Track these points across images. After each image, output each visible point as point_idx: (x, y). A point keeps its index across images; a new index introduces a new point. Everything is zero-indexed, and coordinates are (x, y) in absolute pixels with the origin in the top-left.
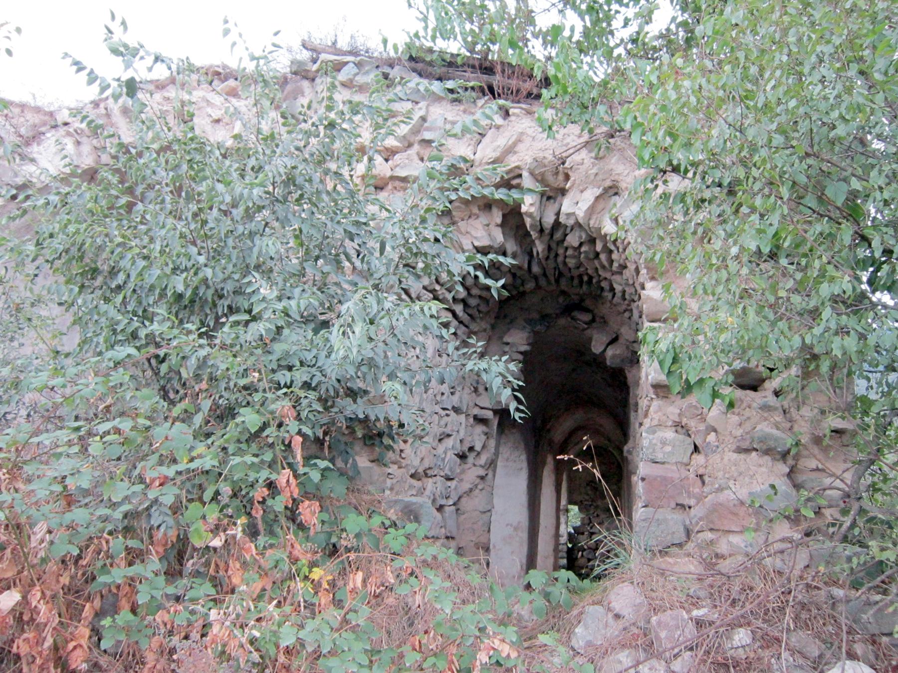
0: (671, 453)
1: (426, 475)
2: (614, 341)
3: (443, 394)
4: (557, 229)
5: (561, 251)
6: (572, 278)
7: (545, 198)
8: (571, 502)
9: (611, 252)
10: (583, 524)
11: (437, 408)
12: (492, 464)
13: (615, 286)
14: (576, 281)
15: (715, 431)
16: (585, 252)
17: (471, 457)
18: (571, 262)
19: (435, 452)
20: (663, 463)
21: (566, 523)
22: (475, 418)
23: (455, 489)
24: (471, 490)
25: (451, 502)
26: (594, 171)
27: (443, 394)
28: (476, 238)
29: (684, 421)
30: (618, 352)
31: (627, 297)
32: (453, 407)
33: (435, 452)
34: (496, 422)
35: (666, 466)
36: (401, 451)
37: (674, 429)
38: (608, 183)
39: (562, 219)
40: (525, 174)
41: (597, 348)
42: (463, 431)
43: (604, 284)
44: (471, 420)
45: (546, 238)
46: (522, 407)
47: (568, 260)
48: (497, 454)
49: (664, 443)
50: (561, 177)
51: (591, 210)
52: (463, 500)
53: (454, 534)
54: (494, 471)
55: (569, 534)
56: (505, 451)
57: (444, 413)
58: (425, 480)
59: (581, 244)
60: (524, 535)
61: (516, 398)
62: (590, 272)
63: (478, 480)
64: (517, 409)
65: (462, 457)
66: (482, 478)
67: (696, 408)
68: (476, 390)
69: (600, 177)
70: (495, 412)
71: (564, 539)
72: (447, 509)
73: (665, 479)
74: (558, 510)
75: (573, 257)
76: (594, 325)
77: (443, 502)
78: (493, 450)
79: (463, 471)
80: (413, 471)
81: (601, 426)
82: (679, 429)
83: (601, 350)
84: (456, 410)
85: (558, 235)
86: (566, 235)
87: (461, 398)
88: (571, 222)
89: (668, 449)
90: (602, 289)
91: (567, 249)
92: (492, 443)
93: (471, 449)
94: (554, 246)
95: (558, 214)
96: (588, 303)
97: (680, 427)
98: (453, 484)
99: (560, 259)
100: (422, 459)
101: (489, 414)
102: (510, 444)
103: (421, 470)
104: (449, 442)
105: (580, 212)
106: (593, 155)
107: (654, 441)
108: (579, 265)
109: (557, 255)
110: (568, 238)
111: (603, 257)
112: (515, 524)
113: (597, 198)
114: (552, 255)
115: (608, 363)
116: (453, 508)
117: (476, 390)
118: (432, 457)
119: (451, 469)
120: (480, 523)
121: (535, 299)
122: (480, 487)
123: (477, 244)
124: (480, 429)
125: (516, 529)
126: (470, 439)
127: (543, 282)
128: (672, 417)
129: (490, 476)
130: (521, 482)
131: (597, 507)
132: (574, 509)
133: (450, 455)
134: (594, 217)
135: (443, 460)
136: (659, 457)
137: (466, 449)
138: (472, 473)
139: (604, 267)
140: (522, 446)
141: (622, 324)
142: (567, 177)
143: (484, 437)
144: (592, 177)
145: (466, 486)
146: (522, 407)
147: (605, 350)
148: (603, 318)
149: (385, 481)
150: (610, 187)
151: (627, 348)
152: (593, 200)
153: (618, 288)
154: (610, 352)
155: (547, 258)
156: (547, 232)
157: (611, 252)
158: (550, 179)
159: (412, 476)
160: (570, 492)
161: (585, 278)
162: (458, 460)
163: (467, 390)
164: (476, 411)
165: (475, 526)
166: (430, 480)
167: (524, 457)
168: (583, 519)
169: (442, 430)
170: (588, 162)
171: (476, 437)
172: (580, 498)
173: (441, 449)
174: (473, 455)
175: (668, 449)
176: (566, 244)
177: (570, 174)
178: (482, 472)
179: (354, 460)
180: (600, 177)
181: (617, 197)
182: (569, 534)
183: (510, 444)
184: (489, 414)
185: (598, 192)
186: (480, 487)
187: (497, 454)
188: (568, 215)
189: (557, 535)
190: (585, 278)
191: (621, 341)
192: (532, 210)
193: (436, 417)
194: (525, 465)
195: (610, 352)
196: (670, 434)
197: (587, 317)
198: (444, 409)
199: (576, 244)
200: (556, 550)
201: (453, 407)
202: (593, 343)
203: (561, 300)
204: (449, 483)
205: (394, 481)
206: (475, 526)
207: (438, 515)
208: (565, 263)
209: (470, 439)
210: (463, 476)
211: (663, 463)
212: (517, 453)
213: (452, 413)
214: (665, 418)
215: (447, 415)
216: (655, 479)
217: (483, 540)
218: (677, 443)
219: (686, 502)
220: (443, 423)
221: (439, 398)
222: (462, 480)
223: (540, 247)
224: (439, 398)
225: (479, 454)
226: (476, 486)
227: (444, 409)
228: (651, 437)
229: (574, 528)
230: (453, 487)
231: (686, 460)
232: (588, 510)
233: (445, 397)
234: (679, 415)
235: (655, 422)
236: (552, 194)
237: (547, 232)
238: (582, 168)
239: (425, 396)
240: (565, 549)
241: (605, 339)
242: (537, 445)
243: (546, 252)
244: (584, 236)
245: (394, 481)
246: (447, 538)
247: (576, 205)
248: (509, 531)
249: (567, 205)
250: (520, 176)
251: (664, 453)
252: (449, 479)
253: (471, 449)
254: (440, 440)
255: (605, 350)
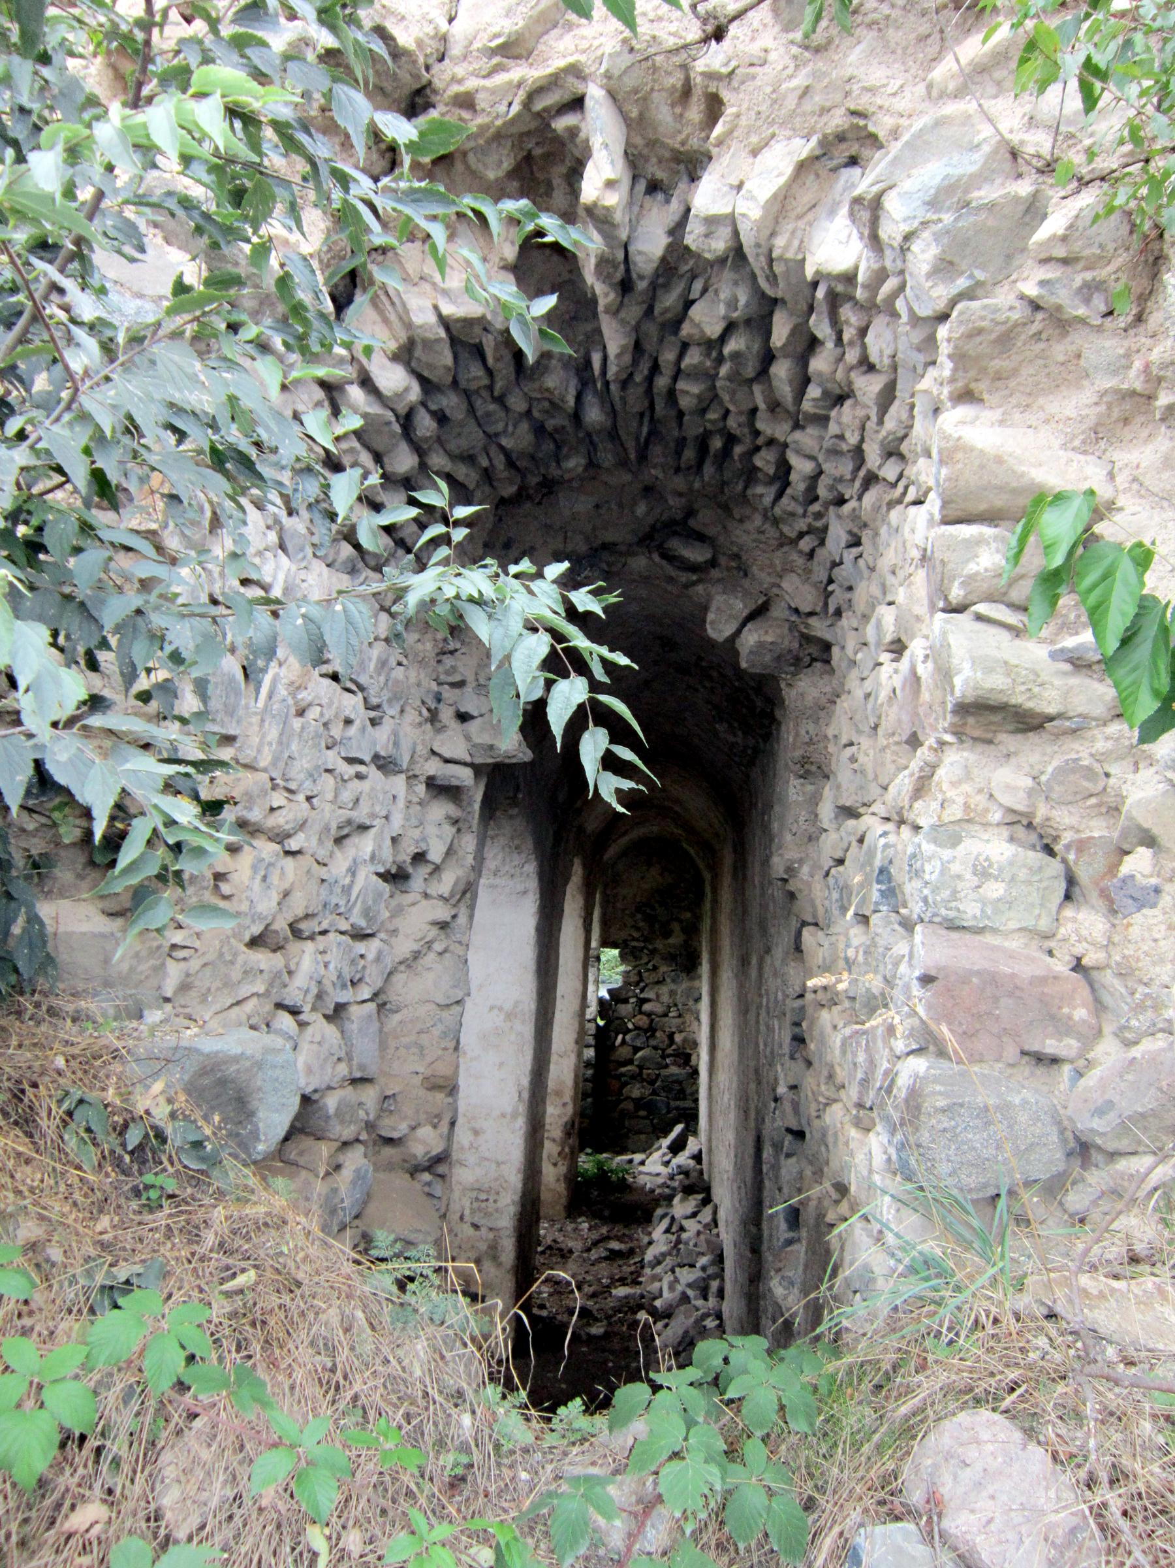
0: (1008, 903)
1: (296, 933)
2: (759, 612)
3: (348, 722)
4: (666, 286)
5: (668, 356)
6: (681, 443)
7: (642, 186)
8: (606, 943)
9: (813, 343)
10: (627, 983)
11: (332, 758)
12: (467, 892)
13: (793, 459)
14: (689, 454)
15: (1150, 841)
16: (736, 355)
17: (419, 876)
18: (690, 391)
19: (323, 872)
20: (980, 931)
21: (597, 982)
22: (431, 782)
23: (378, 959)
24: (417, 955)
25: (366, 993)
26: (800, 81)
27: (348, 722)
28: (445, 293)
29: (1042, 811)
30: (769, 639)
31: (822, 491)
32: (376, 757)
33: (323, 872)
34: (479, 796)
35: (989, 939)
36: (219, 877)
37: (1005, 832)
38: (837, 121)
39: (692, 237)
40: (595, 93)
41: (719, 627)
42: (400, 814)
43: (765, 461)
44: (421, 789)
45: (634, 312)
46: (625, 753)
47: (681, 385)
48: (478, 868)
49: (983, 873)
50: (695, 112)
51: (781, 205)
52: (399, 978)
53: (372, 1071)
54: (472, 908)
55: (601, 1001)
56: (494, 856)
57: (350, 770)
58: (294, 947)
59: (730, 327)
60: (527, 1029)
61: (605, 718)
62: (732, 423)
63: (434, 932)
64: (610, 762)
65: (396, 877)
66: (443, 926)
67: (1089, 773)
68: (433, 717)
69: (818, 99)
70: (477, 769)
71: (592, 1011)
72: (355, 1011)
73: (992, 979)
74: (589, 959)
75: (696, 374)
76: (715, 573)
77: (344, 996)
78: (470, 860)
79: (398, 912)
80: (256, 929)
81: (677, 801)
82: (1020, 832)
83: (728, 630)
84: (385, 764)
85: (669, 300)
86: (688, 304)
87: (395, 734)
88: (719, 245)
89: (995, 890)
90: (751, 474)
91: (685, 346)
92: (469, 843)
93: (419, 857)
94: (651, 329)
95: (678, 229)
96: (705, 519)
97: (1023, 824)
98: (371, 948)
99: (662, 382)
100: (286, 894)
101: (465, 776)
102: (502, 841)
103: (281, 925)
104: (365, 845)
105: (751, 210)
106: (798, 36)
107: (955, 868)
108: (711, 398)
109: (655, 368)
110: (695, 312)
111: (781, 370)
112: (508, 1006)
113: (802, 167)
114: (645, 367)
115: (744, 665)
116: (372, 1006)
117: (433, 717)
118: (313, 885)
119: (366, 913)
120: (436, 1032)
121: (582, 504)
122: (438, 947)
123: (447, 309)
124: (440, 810)
125: (510, 1016)
126: (416, 834)
127: (606, 457)
128: (1007, 800)
129: (462, 920)
130: (522, 918)
131: (653, 952)
132: (611, 954)
133: (366, 878)
134: (787, 227)
135: (347, 890)
136: (970, 910)
137: (405, 857)
138: (418, 915)
139: (775, 406)
140: (529, 844)
141: (788, 569)
142: (714, 107)
143: (449, 831)
144: (791, 102)
145: (404, 947)
146: (625, 753)
147: (739, 632)
148: (737, 556)
149: (160, 969)
150: (841, 138)
151: (793, 627)
152: (789, 170)
153: (801, 467)
154: (750, 638)
155: (625, 384)
156: (642, 285)
157: (813, 343)
158: (663, 114)
159: (255, 942)
160: (605, 923)
161: (717, 443)
162: (386, 888)
163: (411, 716)
164: (433, 767)
165: (425, 1039)
166: (309, 946)
167: (531, 868)
168: (626, 974)
169: (345, 814)
170: (780, 57)
171: (431, 830)
172: (623, 935)
173: (340, 865)
174: (423, 871)
175: (995, 890)
176: (686, 330)
177: (725, 95)
178: (442, 912)
179: (34, 919)
180: (818, 99)
181: (856, 171)
182: (601, 1001)
183: (502, 841)
184: (465, 776)
185: (804, 148)
186: (438, 947)
187: (478, 868)
188: (712, 221)
189: (584, 1005)
190: (717, 443)
191: (778, 611)
192: (612, 199)
193: (329, 781)
194: (533, 884)
195: (750, 638)
196: (998, 848)
197: (696, 554)
198: (351, 761)
199: (714, 329)
200: (582, 1032)
201: (376, 757)
202: (711, 616)
203: (641, 509)
204: (361, 947)
205: (195, 964)
206: (425, 1039)
207: (331, 1031)
208: (672, 395)
209: (416, 834)
210: (397, 922)
211: (980, 931)
212: (517, 859)
213: (372, 771)
214: (981, 800)
215: (360, 776)
216: (965, 980)
217: (442, 1069)
218: (1023, 874)
219: (1051, 1046)
220: (347, 796)
221: (337, 731)
222: (394, 932)
223: (615, 340)
224: (337, 731)
225: (437, 868)
226: (429, 945)
227: (351, 761)
228: (947, 854)
229: (610, 991)
230: (370, 956)
231: (1044, 924)
232: (636, 958)
233: (353, 731)
234: (1030, 793)
235: (955, 812)
236: (665, 168)
237: (642, 285)
238: (765, 75)
239: (297, 723)
240: (593, 1031)
241: (740, 607)
242: (558, 840)
243: (627, 359)
244: (743, 299)
245: (195, 964)
246: (354, 1081)
247: (737, 189)
248: (498, 1019)
249: (708, 196)
250: (577, 103)
251: (984, 902)
252: (360, 936)
253: (419, 857)
254: (339, 841)
255: (739, 632)
